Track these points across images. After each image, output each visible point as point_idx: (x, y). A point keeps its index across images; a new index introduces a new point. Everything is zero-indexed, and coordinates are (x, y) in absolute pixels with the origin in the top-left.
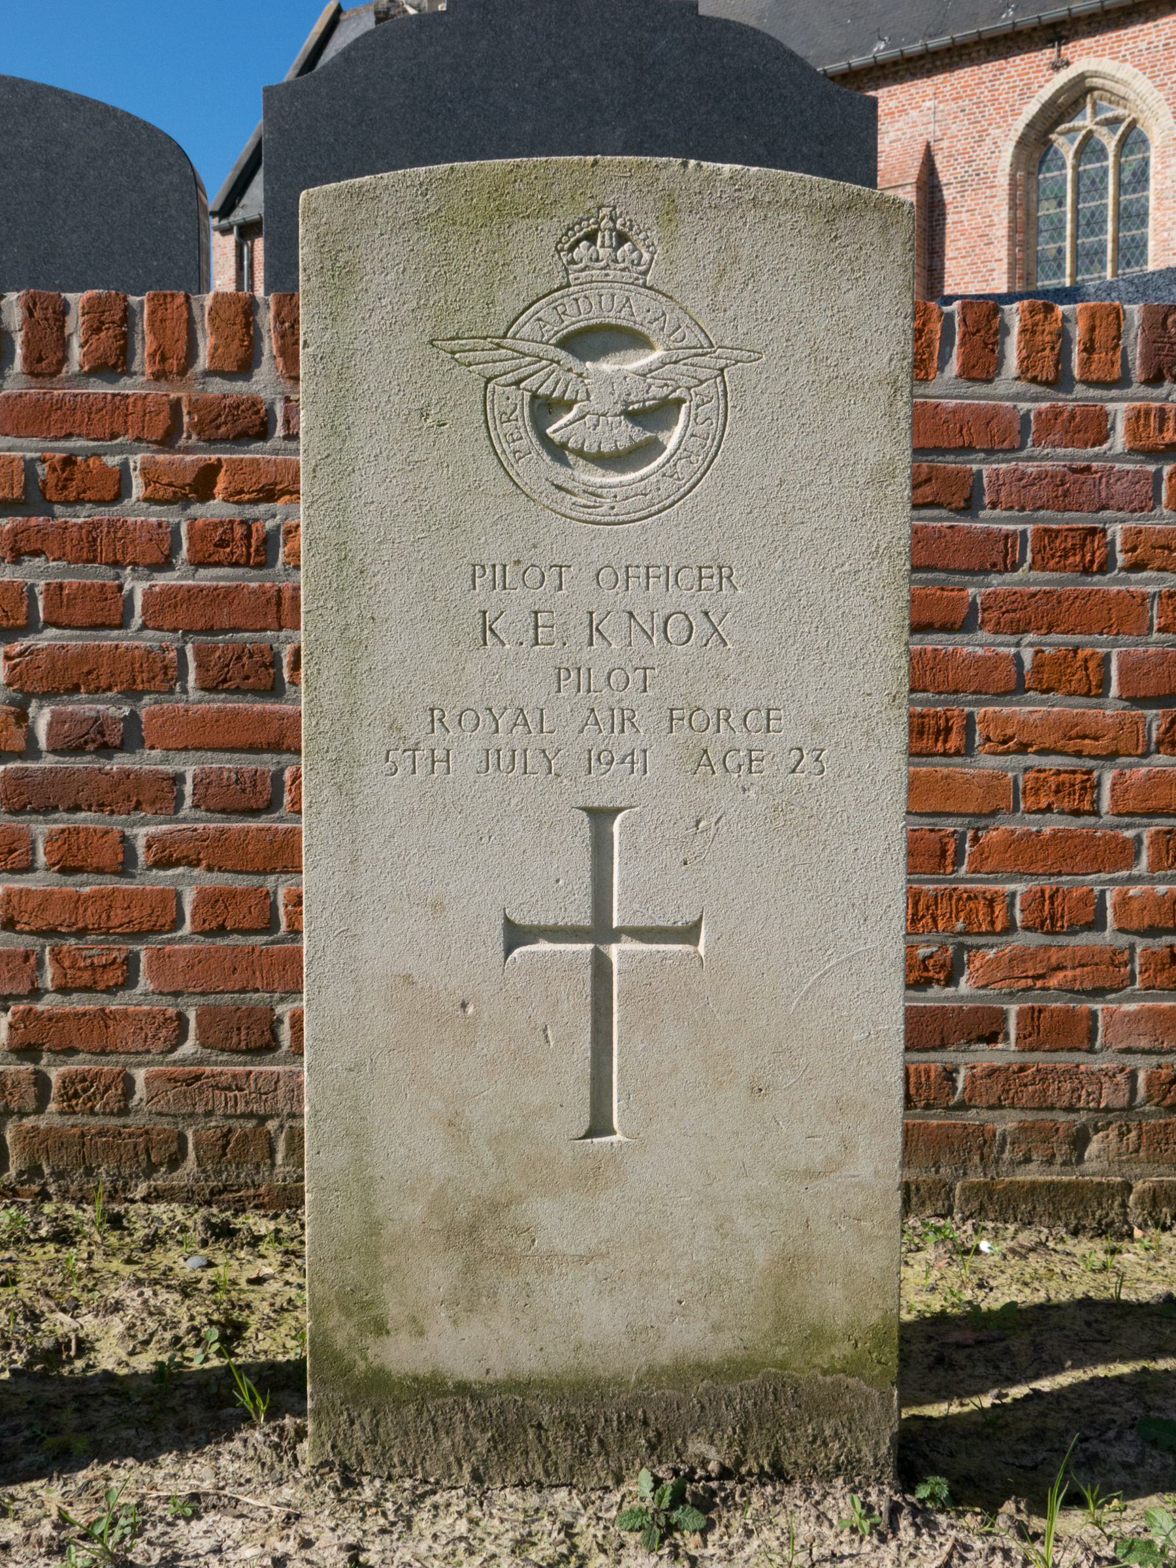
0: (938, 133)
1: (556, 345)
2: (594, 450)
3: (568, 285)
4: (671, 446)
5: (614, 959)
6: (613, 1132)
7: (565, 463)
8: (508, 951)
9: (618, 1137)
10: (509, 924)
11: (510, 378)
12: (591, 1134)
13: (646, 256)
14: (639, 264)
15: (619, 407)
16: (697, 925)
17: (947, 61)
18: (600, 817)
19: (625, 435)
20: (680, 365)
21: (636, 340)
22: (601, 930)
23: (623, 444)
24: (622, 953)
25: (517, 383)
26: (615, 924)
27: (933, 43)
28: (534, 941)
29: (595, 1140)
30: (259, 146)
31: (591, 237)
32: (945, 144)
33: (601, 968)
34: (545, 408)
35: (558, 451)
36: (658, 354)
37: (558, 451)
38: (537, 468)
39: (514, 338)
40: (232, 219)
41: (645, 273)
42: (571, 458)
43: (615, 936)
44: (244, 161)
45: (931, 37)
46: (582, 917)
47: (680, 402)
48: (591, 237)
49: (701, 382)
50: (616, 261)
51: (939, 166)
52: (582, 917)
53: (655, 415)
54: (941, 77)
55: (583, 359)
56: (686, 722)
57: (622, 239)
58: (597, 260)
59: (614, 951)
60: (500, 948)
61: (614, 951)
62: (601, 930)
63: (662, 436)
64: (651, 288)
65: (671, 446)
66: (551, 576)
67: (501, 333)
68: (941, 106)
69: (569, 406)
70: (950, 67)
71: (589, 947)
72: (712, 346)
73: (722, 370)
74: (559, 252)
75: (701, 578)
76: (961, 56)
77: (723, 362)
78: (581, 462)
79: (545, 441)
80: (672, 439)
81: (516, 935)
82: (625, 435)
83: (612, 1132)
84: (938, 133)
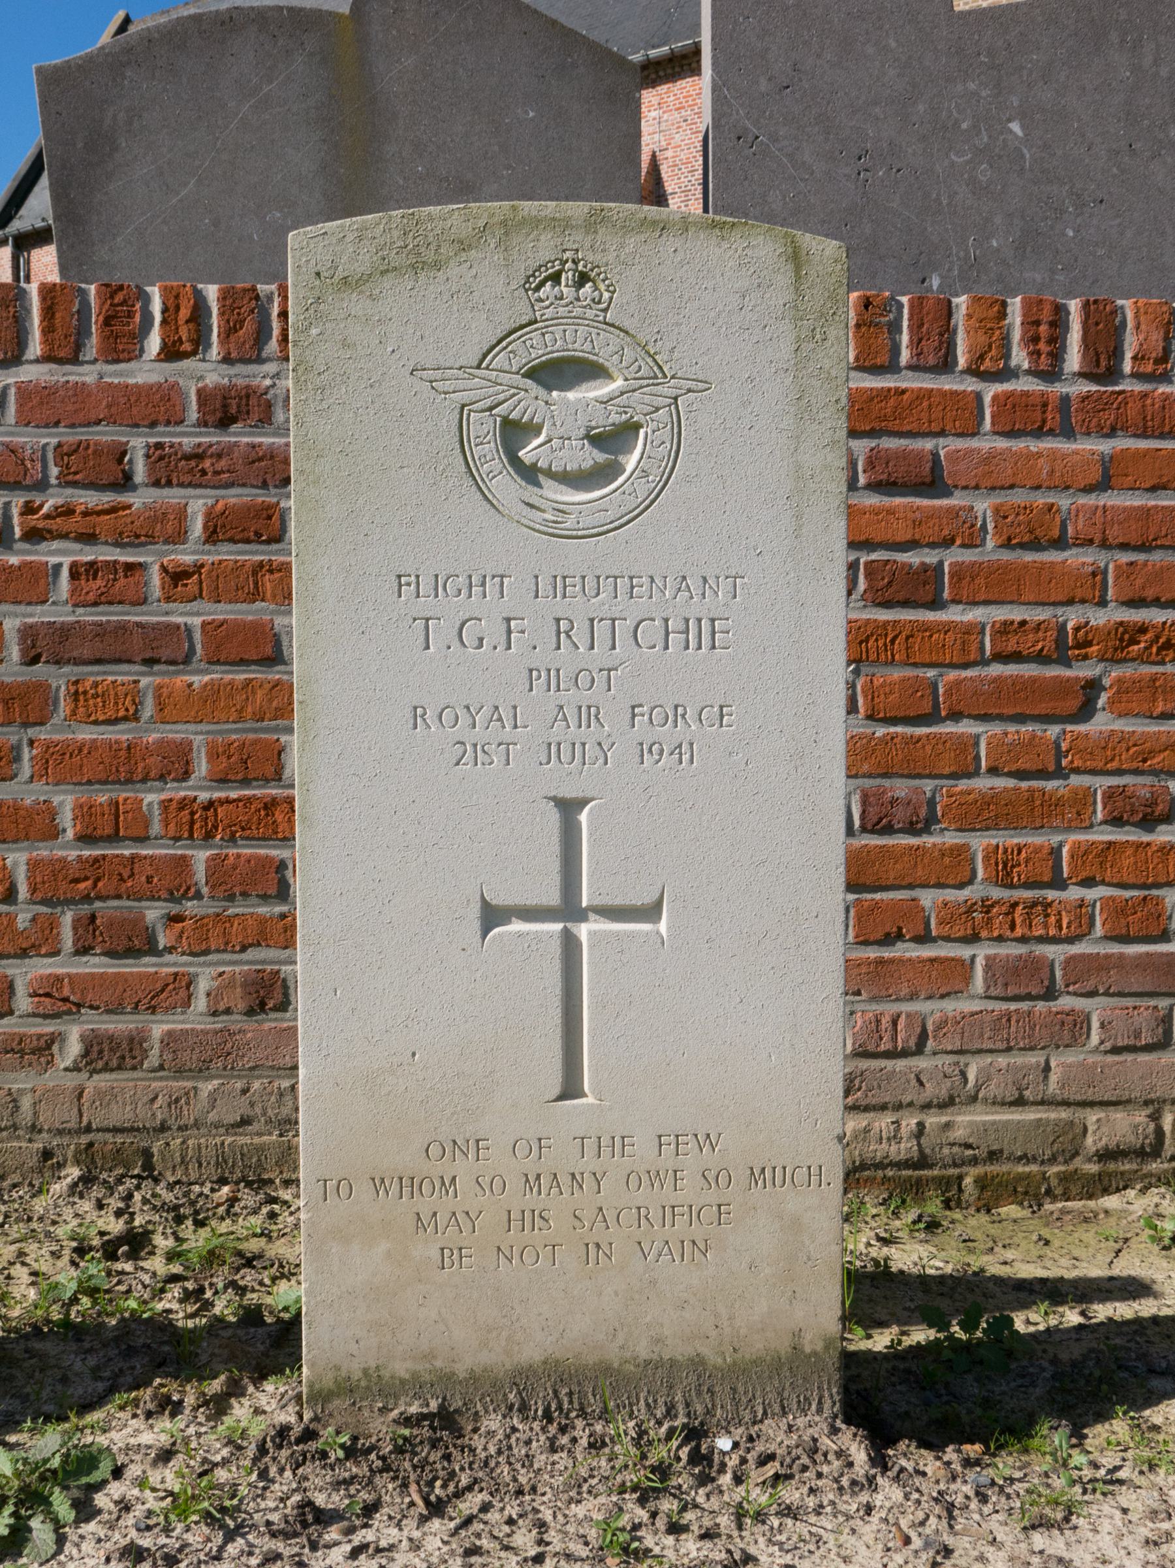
0: (664, 143)
1: (524, 376)
2: (560, 469)
3: (536, 322)
4: (629, 468)
5: (584, 938)
6: (584, 1095)
7: (538, 485)
8: (485, 931)
9: (590, 1100)
10: (486, 906)
11: (488, 403)
12: (561, 1098)
13: (606, 295)
14: (599, 302)
15: (583, 431)
16: (658, 905)
17: (669, 71)
18: (568, 808)
19: (591, 457)
20: (636, 394)
21: (591, 371)
22: (569, 909)
23: (587, 464)
24: (591, 934)
25: (491, 409)
26: (584, 904)
27: (653, 53)
28: (507, 921)
29: (568, 1102)
30: (39, 156)
31: (556, 278)
32: (669, 154)
33: (570, 944)
34: (514, 432)
35: (530, 474)
36: (619, 383)
37: (530, 474)
38: (506, 486)
39: (487, 368)
40: (7, 230)
41: (605, 310)
42: (541, 478)
43: (581, 915)
44: (23, 172)
45: (654, 47)
46: (551, 896)
47: (637, 427)
48: (556, 278)
49: (657, 409)
50: (578, 299)
51: (664, 176)
52: (551, 896)
53: (613, 439)
54: (665, 87)
55: (549, 388)
56: (646, 717)
57: (583, 279)
58: (561, 298)
59: (583, 931)
60: (477, 925)
61: (583, 931)
62: (569, 909)
63: (620, 458)
64: (612, 325)
65: (629, 468)
66: (725, 586)
67: (475, 364)
68: (666, 116)
69: (538, 430)
70: (672, 77)
71: (558, 927)
72: (665, 376)
73: (676, 399)
74: (527, 291)
75: (632, 587)
76: (682, 66)
77: (675, 392)
78: (551, 482)
79: (515, 461)
80: (631, 462)
81: (492, 916)
82: (591, 457)
83: (584, 1095)
84: (664, 143)
